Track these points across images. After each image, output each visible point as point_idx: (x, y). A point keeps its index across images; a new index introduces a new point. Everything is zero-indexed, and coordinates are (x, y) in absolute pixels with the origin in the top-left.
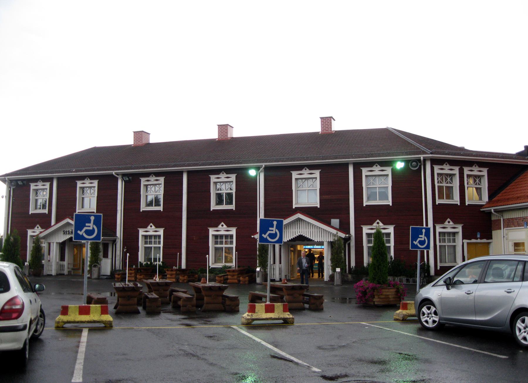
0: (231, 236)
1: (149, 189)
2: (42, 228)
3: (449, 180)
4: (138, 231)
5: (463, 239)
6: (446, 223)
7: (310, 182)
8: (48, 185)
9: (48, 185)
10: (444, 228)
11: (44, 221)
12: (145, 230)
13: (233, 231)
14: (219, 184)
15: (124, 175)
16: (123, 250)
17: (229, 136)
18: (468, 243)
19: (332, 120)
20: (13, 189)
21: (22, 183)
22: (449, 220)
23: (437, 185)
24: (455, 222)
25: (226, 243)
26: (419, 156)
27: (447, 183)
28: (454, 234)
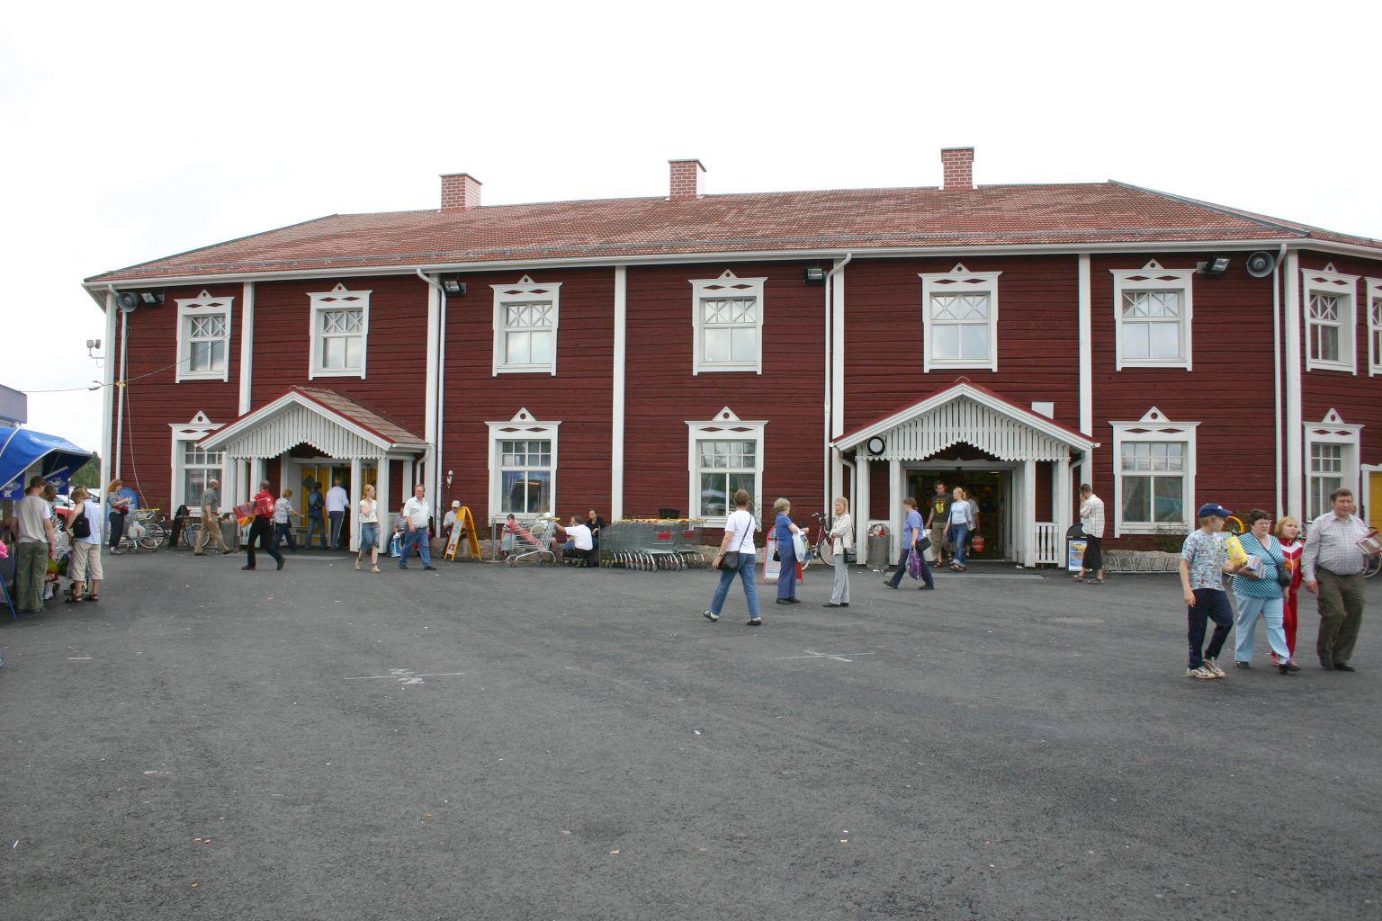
0: (546, 444)
1: (512, 316)
2: (213, 419)
3: (1329, 310)
4: (687, 428)
5: (1363, 461)
6: (1327, 420)
7: (537, 312)
8: (226, 304)
9: (226, 304)
10: (1322, 432)
11: (217, 401)
12: (707, 424)
13: (551, 431)
14: (514, 308)
15: (444, 277)
16: (444, 481)
17: (469, 203)
18: (1372, 474)
19: (698, 167)
20: (128, 314)
21: (152, 299)
22: (1154, 410)
23: (1309, 321)
24: (539, 416)
25: (533, 460)
26: (414, 266)
27: (1326, 317)
28: (1337, 448)
